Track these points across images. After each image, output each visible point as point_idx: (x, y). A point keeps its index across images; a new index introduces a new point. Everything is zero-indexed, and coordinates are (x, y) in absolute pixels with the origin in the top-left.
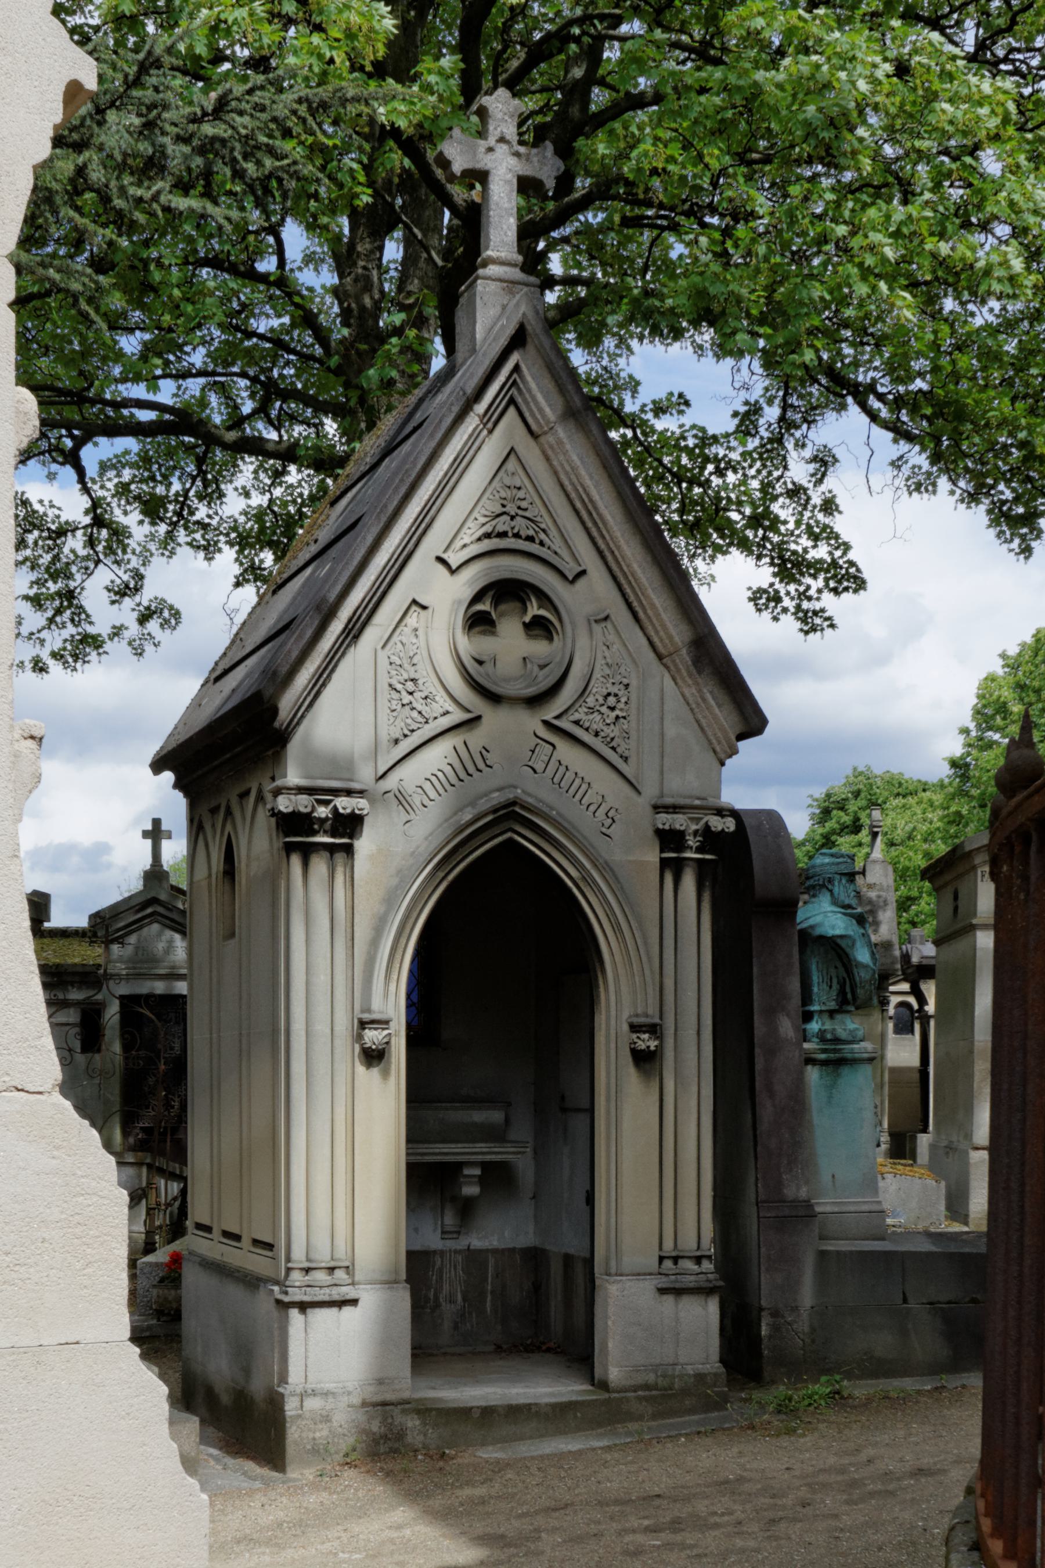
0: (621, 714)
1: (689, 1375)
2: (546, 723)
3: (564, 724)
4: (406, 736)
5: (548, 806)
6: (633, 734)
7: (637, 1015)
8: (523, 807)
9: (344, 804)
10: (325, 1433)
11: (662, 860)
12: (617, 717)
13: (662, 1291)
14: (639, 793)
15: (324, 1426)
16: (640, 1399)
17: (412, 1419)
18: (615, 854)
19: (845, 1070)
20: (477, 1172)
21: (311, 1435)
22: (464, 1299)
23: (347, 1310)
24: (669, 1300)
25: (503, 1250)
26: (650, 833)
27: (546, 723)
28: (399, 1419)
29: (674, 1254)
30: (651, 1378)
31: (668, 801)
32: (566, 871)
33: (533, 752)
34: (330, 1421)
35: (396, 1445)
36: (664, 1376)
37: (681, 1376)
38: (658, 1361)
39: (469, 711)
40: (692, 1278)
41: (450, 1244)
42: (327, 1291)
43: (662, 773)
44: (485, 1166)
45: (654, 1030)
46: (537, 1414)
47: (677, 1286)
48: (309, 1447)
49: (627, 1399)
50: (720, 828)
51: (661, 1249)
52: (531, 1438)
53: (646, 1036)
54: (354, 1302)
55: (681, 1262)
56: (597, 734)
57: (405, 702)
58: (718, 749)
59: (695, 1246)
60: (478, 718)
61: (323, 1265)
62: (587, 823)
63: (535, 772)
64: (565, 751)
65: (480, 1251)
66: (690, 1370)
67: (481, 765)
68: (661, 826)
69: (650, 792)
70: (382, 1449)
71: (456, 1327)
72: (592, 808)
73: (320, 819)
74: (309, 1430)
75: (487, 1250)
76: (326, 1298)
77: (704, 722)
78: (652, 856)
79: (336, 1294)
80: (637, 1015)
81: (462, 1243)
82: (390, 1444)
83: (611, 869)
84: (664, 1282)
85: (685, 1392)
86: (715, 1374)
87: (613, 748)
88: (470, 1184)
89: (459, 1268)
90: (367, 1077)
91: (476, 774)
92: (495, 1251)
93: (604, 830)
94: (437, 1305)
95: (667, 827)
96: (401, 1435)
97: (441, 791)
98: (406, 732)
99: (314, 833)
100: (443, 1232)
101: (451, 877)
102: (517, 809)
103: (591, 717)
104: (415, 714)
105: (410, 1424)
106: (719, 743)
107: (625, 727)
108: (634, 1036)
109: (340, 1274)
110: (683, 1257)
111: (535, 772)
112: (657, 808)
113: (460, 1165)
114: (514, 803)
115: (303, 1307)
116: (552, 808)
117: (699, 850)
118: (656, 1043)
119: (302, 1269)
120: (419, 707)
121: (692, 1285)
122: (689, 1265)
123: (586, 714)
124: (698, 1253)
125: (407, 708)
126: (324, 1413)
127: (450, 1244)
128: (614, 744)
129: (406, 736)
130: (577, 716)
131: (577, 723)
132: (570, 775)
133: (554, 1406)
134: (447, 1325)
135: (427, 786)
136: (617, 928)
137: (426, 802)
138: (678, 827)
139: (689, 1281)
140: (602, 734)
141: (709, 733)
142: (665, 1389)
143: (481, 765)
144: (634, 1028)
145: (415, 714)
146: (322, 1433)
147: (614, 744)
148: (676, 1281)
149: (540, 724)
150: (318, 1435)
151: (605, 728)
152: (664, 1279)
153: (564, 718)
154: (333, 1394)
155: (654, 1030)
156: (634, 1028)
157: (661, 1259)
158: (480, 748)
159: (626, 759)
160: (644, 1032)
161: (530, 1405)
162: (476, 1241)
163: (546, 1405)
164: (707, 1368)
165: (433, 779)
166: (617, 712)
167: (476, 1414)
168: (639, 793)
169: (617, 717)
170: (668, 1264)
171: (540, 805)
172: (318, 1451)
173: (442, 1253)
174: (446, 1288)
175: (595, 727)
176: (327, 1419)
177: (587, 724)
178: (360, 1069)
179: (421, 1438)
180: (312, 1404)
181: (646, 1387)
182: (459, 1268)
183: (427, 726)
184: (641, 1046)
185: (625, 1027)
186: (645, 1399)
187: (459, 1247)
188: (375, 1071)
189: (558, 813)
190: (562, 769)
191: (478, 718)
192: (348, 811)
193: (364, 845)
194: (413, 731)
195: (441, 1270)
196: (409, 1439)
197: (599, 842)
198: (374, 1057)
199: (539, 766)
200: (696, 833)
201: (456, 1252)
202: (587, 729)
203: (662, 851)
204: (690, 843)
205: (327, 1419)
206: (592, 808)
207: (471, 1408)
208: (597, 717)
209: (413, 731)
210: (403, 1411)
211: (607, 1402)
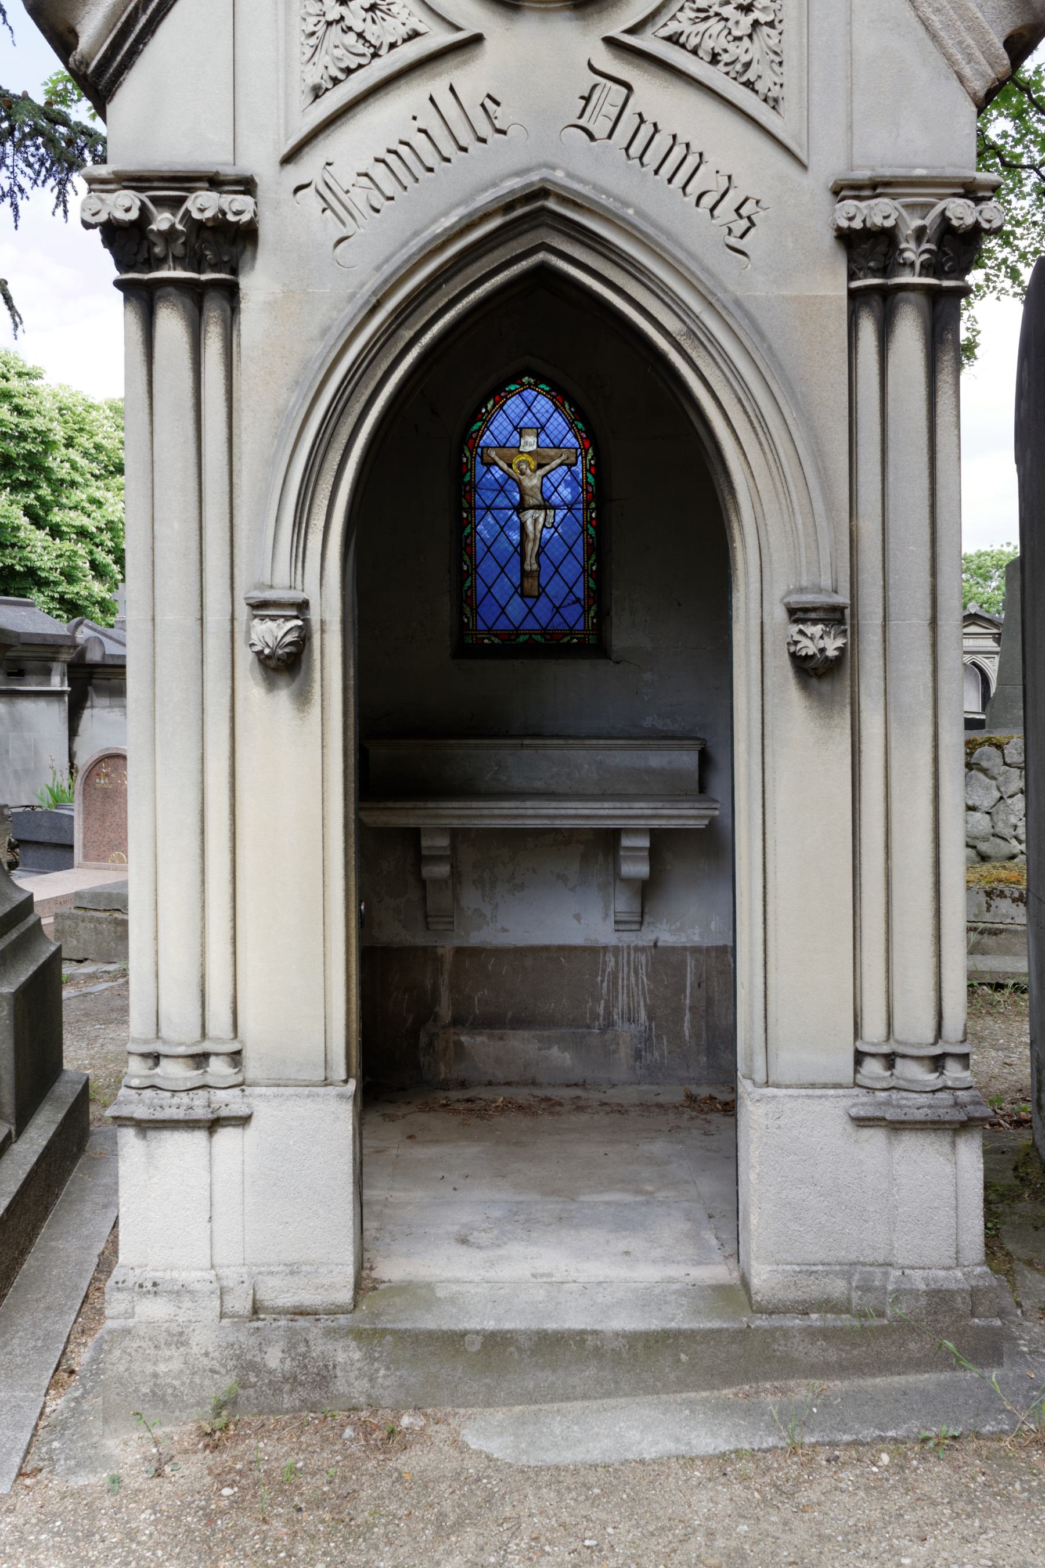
0: (763, 18)
1: (914, 1293)
2: (610, 42)
3: (648, 42)
4: (336, 81)
5: (616, 199)
6: (791, 57)
7: (801, 590)
8: (564, 200)
9: (204, 204)
10: (176, 1365)
11: (852, 294)
12: (756, 24)
13: (861, 1122)
14: (804, 166)
15: (173, 1351)
16: (812, 1334)
17: (346, 1349)
18: (752, 282)
19: (638, 1102)
20: (645, 842)
21: (149, 1369)
22: (650, 1018)
23: (226, 1136)
24: (877, 1137)
25: (708, 949)
26: (827, 239)
27: (610, 42)
28: (319, 1347)
29: (885, 1049)
30: (837, 1288)
31: (863, 174)
32: (656, 322)
33: (587, 99)
34: (185, 1344)
35: (315, 1396)
36: (866, 1288)
37: (899, 1295)
38: (852, 1257)
39: (458, 29)
40: (923, 1099)
41: (629, 939)
42: (184, 1099)
43: (850, 127)
44: (655, 834)
45: (835, 617)
46: (598, 1352)
47: (890, 1114)
48: (145, 1390)
49: (786, 1333)
50: (969, 221)
51: (857, 1033)
52: (585, 1397)
53: (817, 629)
54: (243, 1121)
55: (902, 1067)
56: (714, 59)
57: (330, 17)
58: (967, 71)
59: (929, 1035)
60: (477, 40)
61: (181, 1050)
62: (696, 232)
63: (592, 137)
64: (652, 94)
65: (673, 949)
66: (918, 1280)
67: (484, 129)
68: (844, 224)
69: (829, 164)
70: (288, 1401)
71: (638, 1056)
72: (708, 201)
73: (160, 233)
74: (147, 1359)
75: (685, 949)
76: (180, 1114)
77: (936, 21)
78: (832, 283)
79: (199, 1106)
80: (801, 590)
81: (646, 937)
82: (302, 1392)
83: (747, 315)
84: (863, 1104)
85: (905, 1327)
86: (974, 1292)
87: (749, 84)
88: (635, 860)
89: (642, 972)
90: (264, 707)
91: (474, 146)
92: (696, 950)
93: (733, 241)
94: (610, 1024)
95: (857, 224)
96: (324, 1378)
97: (407, 180)
98: (335, 72)
99: (158, 263)
100: (616, 922)
101: (426, 339)
102: (551, 204)
103: (702, 27)
104: (351, 38)
105: (341, 1357)
106: (970, 58)
107: (773, 42)
108: (795, 628)
109: (218, 1067)
110: (904, 1056)
111: (592, 137)
112: (840, 191)
113: (615, 835)
114: (542, 193)
115: (145, 1127)
116: (626, 204)
117: (927, 269)
118: (839, 642)
119: (144, 1056)
120: (358, 27)
121: (919, 1115)
122: (912, 1072)
123: (694, 21)
124: (937, 1051)
125: (336, 29)
126: (175, 1329)
127: (629, 939)
128: (750, 75)
129: (336, 81)
130: (673, 27)
131: (673, 39)
132: (661, 142)
133: (633, 1338)
134: (624, 1052)
135: (379, 172)
136: (757, 422)
137: (378, 201)
138: (878, 221)
139: (916, 1106)
140: (725, 58)
141: (949, 42)
142: (863, 1315)
143: (484, 129)
144: (797, 614)
145: (351, 38)
146: (169, 1365)
147: (750, 75)
148: (888, 1103)
149: (601, 46)
150: (162, 1368)
151: (731, 47)
152: (864, 1097)
153: (649, 31)
154: (191, 1292)
155: (835, 617)
156: (797, 614)
157: (859, 1057)
158: (482, 98)
159: (774, 103)
160: (815, 622)
161: (583, 1332)
162: (665, 933)
163: (617, 1334)
164: (955, 1279)
165: (391, 159)
166: (756, 15)
167: (475, 1345)
168: (804, 166)
169: (756, 24)
170: (873, 1068)
171: (603, 199)
172: (163, 1399)
173: (616, 950)
174: (622, 999)
175: (708, 44)
176: (179, 1339)
177: (693, 42)
178: (252, 688)
179: (365, 1384)
180: (154, 1310)
181: (827, 1306)
182: (642, 972)
183: (377, 62)
184: (808, 648)
185: (780, 614)
186: (826, 1334)
187: (640, 943)
188: (283, 697)
189: (638, 212)
190: (646, 131)
191: (477, 40)
192: (209, 214)
193: (257, 284)
194: (349, 71)
195: (615, 975)
196: (340, 1386)
197: (724, 264)
198: (286, 665)
199: (600, 127)
200: (920, 234)
201: (637, 949)
202: (694, 52)
203: (852, 276)
204: (909, 255)
205: (179, 1339)
206: (708, 201)
207: (464, 1334)
208: (715, 26)
209: (349, 71)
210: (330, 1333)
211: (743, 1335)
